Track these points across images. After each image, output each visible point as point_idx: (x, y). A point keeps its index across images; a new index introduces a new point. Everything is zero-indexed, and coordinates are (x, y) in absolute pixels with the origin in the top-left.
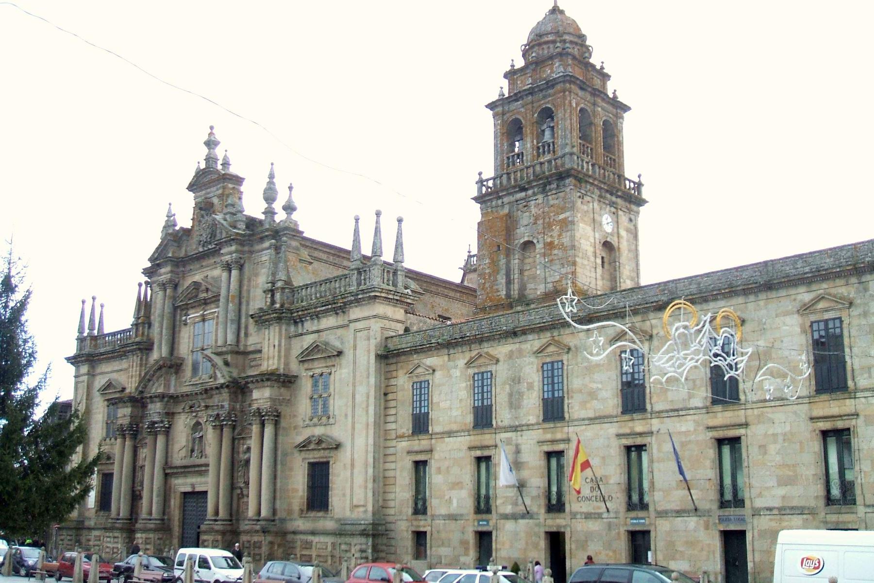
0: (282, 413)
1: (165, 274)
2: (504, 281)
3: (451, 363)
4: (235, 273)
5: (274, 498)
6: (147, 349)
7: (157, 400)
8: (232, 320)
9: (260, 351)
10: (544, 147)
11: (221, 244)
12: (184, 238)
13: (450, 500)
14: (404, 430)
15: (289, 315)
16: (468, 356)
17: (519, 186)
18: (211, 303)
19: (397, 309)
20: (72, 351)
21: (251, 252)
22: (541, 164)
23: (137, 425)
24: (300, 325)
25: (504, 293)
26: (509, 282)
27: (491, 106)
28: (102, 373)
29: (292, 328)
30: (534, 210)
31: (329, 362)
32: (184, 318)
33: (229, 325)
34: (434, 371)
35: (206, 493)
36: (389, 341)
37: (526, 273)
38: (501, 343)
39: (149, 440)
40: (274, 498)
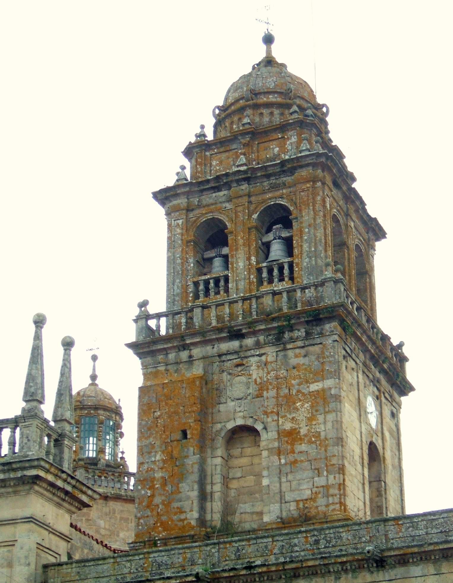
2: (194, 494)
10: (270, 271)
19: (61, 512)
22: (274, 293)
25: (196, 515)
26: (204, 497)
27: (163, 196)
36: (51, 572)
37: (234, 485)
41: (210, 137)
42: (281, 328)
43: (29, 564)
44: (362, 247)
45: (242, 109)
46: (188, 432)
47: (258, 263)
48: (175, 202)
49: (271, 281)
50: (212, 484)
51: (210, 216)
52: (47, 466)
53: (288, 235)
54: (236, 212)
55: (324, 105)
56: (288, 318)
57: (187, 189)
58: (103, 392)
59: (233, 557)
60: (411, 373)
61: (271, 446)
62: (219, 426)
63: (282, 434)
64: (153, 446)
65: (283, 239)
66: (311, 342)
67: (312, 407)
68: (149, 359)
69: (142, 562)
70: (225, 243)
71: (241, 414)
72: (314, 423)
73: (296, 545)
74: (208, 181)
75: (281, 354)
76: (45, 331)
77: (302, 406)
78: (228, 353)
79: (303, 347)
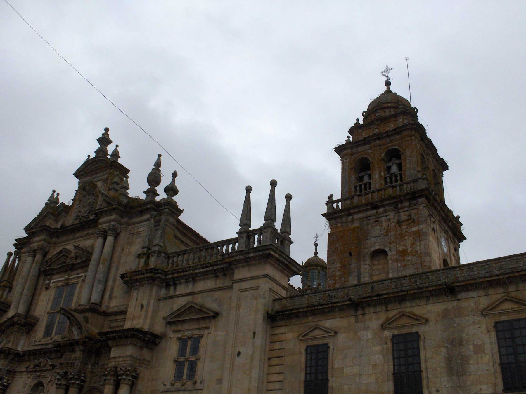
0: (141, 375)
1: (38, 241)
9: (124, 313)
10: (391, 179)
11: (99, 214)
12: (63, 214)
15: (163, 277)
16: (383, 317)
21: (128, 224)
24: (172, 288)
27: (339, 150)
29: (163, 292)
30: (385, 224)
31: (203, 324)
32: (47, 282)
34: (336, 333)
38: (431, 301)
41: (361, 122)
42: (396, 202)
43: (265, 298)
45: (376, 110)
47: (385, 175)
48: (345, 152)
52: (275, 249)
54: (375, 154)
55: (415, 108)
56: (400, 197)
57: (351, 145)
58: (320, 259)
59: (370, 291)
60: (465, 231)
61: (393, 258)
62: (367, 250)
63: (398, 252)
65: (397, 164)
66: (412, 208)
67: (413, 238)
68: (333, 221)
70: (369, 169)
73: (404, 284)
75: (397, 215)
76: (277, 188)
78: (371, 216)
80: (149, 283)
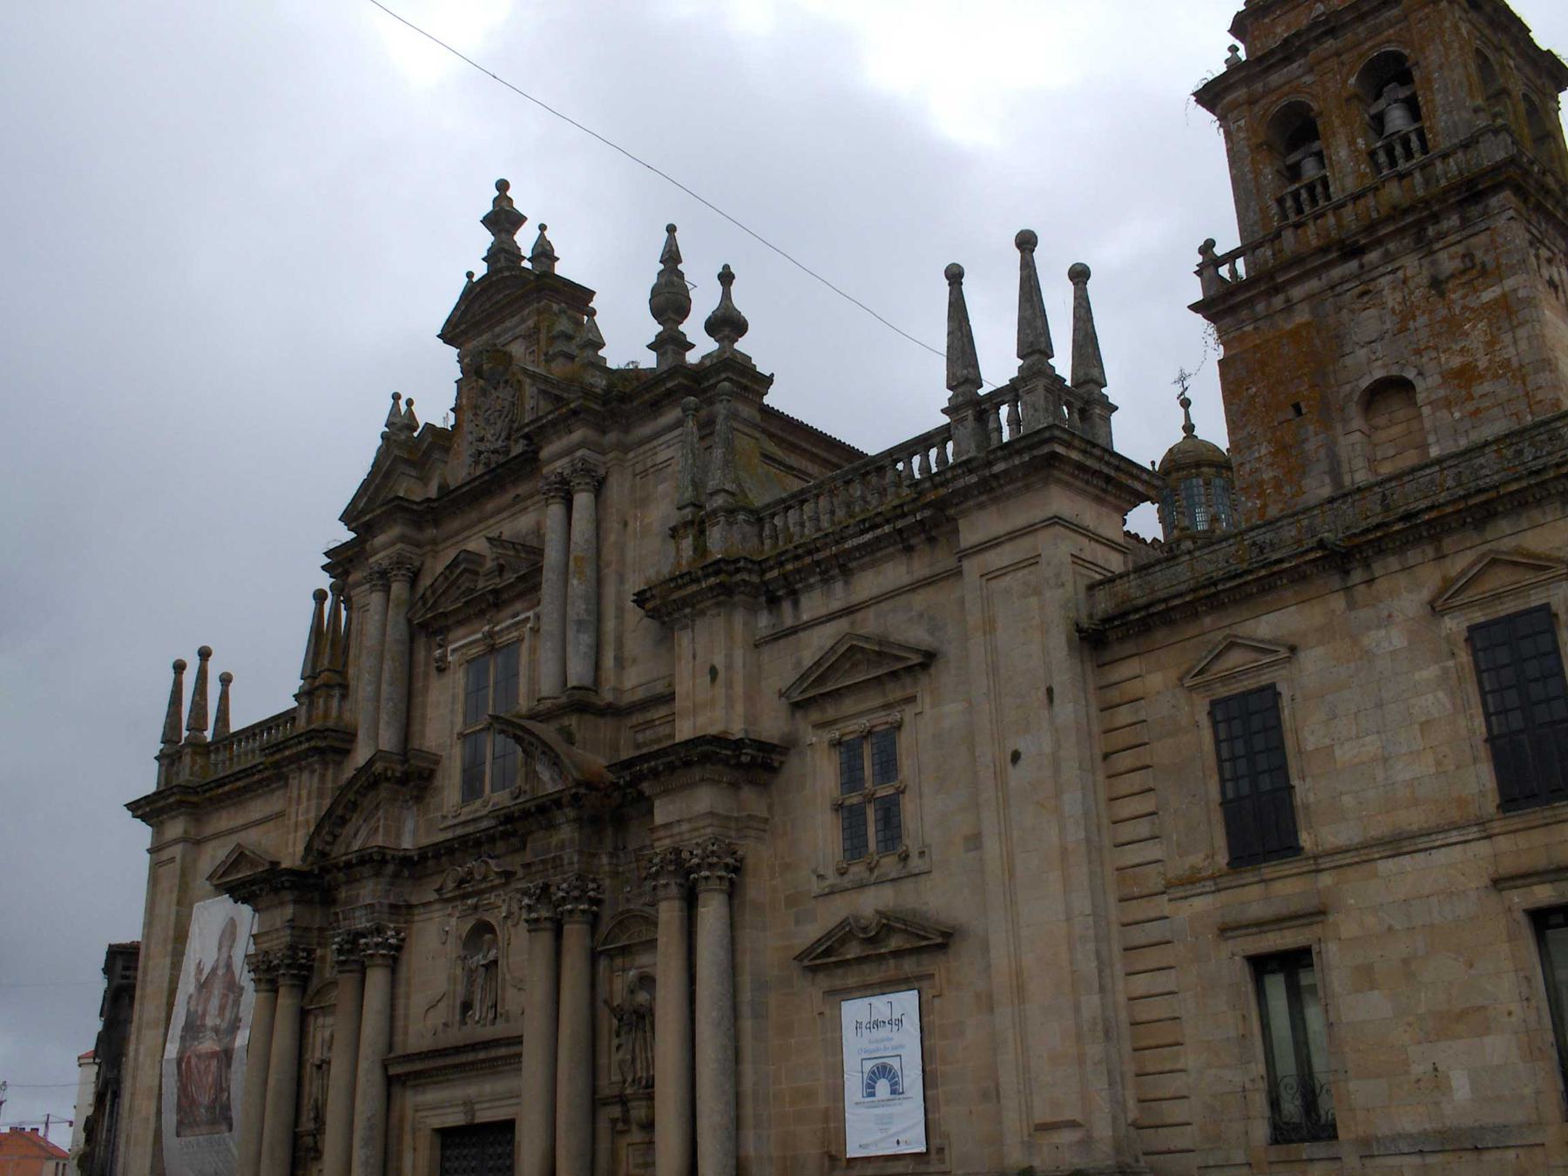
1: (387, 544)
3: (1363, 614)
4: (582, 500)
5: (738, 1122)
6: (335, 750)
7: (367, 870)
8: (580, 623)
9: (669, 698)
10: (1390, 151)
11: (535, 437)
12: (436, 455)
13: (1438, 1079)
14: (1197, 859)
16: (1430, 578)
17: (1341, 243)
18: (511, 601)
20: (146, 782)
21: (625, 449)
23: (310, 952)
24: (787, 607)
27: (1209, 96)
28: (216, 836)
29: (764, 621)
30: (1392, 299)
31: (895, 693)
32: (438, 652)
33: (570, 634)
34: (1293, 649)
35: (508, 1126)
39: (348, 982)
40: (738, 1122)
42: (1416, 224)
44: (1534, 97)
46: (1302, 405)
48: (1229, 98)
49: (1393, 162)
50: (1352, 471)
51: (1284, 102)
52: (1065, 437)
53: (1408, 93)
56: (1426, 203)
57: (1243, 74)
61: (1433, 397)
62: (1348, 388)
64: (1253, 437)
67: (1490, 325)
68: (1228, 320)
69: (1233, 548)
71: (1379, 363)
72: (1497, 347)
73: (1482, 467)
74: (1272, 52)
75: (1426, 262)
77: (1474, 327)
78: (1343, 281)
79: (1459, 242)
80: (719, 604)
